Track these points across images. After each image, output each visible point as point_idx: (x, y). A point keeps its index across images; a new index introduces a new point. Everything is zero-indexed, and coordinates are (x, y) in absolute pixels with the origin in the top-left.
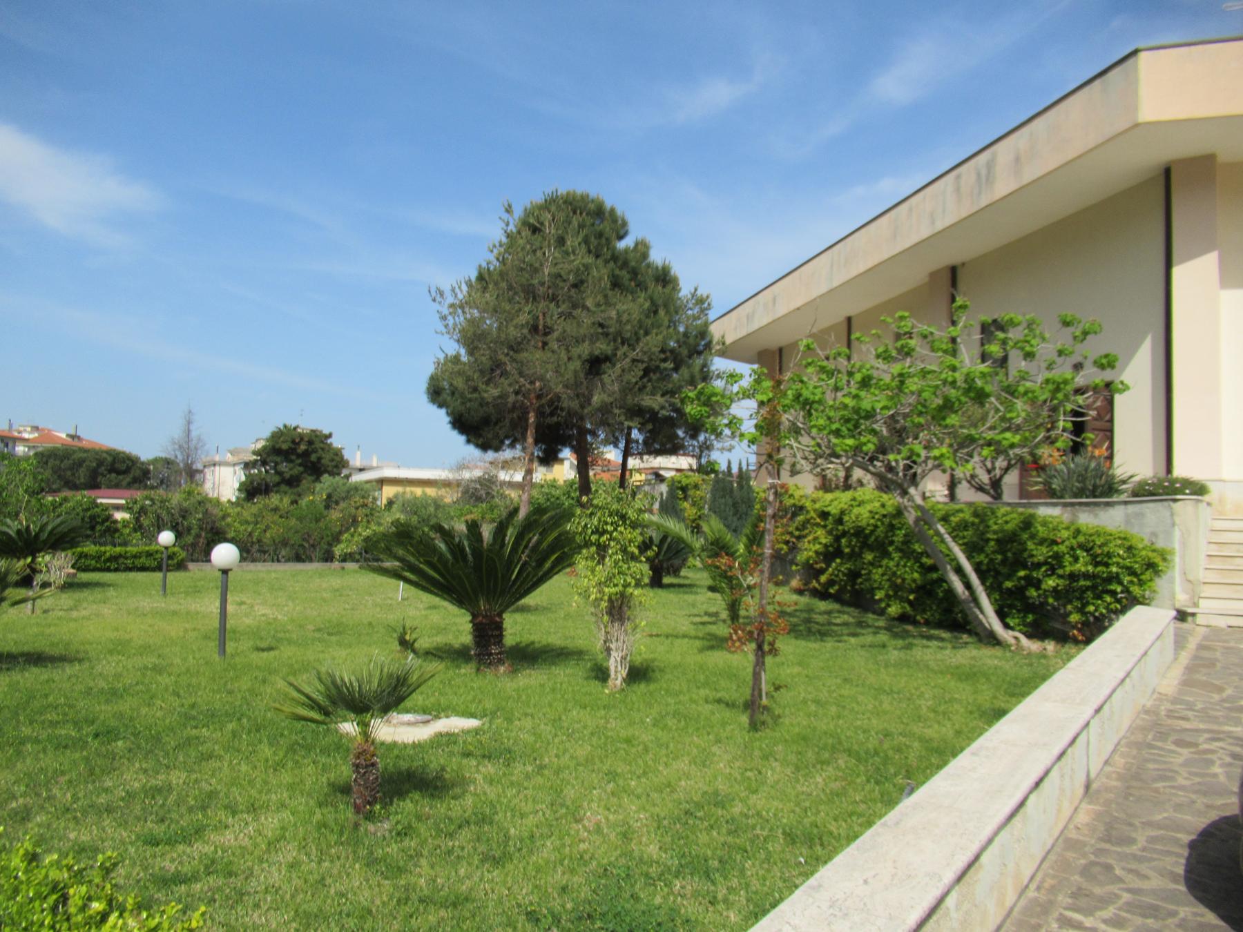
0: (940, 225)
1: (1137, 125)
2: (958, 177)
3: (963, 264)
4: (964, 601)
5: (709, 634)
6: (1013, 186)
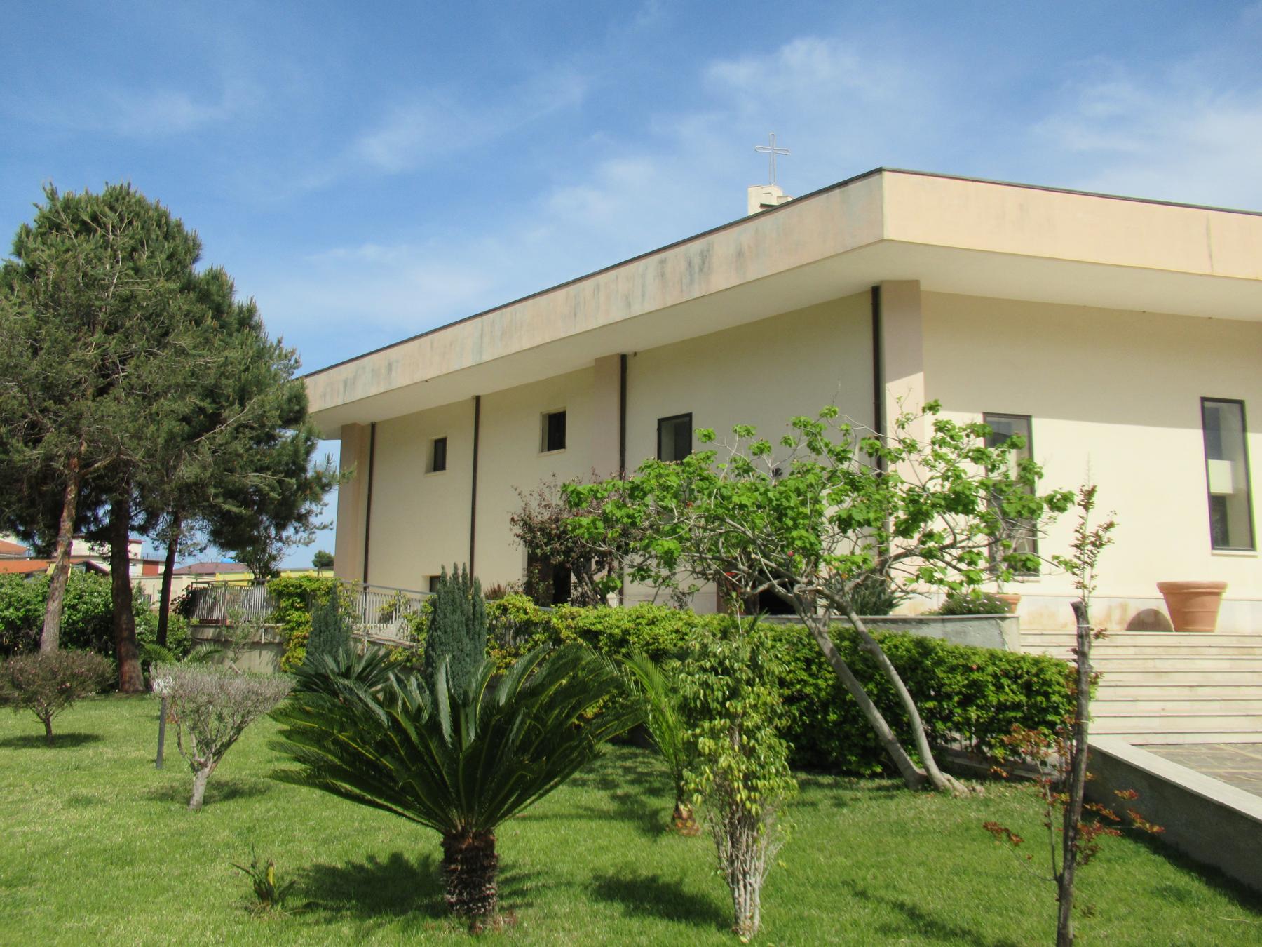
0: (638, 310)
1: (882, 241)
2: (663, 262)
3: (635, 354)
4: (890, 742)
5: (275, 771)
6: (734, 281)
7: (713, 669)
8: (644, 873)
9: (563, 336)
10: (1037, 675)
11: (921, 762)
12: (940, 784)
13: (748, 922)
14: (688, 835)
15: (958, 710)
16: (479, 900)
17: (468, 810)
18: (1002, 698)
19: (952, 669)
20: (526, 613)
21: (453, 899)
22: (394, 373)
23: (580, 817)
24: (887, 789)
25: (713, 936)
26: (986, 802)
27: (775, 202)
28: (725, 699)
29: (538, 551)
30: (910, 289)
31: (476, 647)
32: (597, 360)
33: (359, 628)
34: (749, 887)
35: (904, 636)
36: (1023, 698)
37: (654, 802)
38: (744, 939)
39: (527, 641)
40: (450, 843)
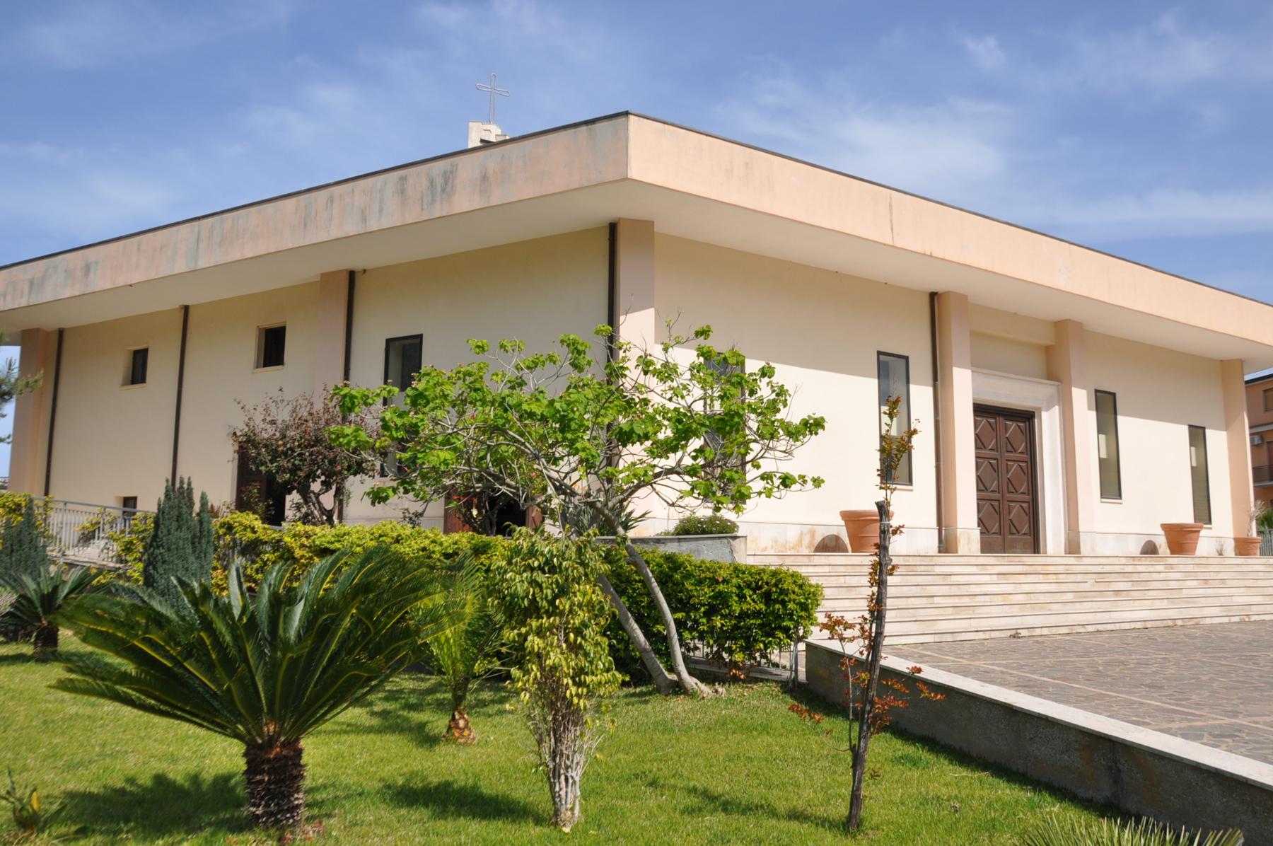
0: (374, 225)
2: (403, 179)
3: (365, 271)
6: (477, 204)
7: (541, 568)
8: (435, 780)
9: (290, 246)
10: (776, 585)
11: (672, 669)
12: (689, 687)
13: (569, 813)
14: (465, 744)
15: (704, 620)
16: (288, 811)
17: (280, 720)
18: (745, 607)
19: (700, 582)
20: (255, 532)
21: (260, 811)
22: (92, 275)
23: (346, 732)
24: (641, 694)
25: (533, 831)
26: (730, 702)
27: (493, 139)
28: (555, 597)
29: (263, 468)
30: (645, 228)
31: (202, 567)
32: (322, 275)
33: (52, 551)
34: (571, 781)
35: (653, 552)
36: (763, 607)
37: (417, 717)
38: (567, 830)
39: (254, 562)
40: (254, 756)
